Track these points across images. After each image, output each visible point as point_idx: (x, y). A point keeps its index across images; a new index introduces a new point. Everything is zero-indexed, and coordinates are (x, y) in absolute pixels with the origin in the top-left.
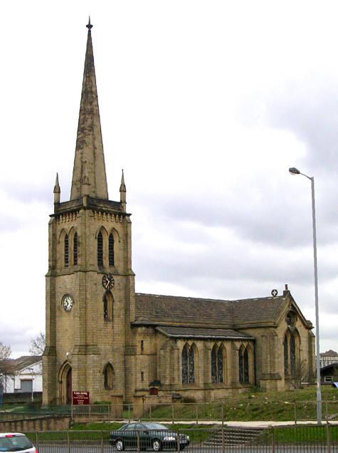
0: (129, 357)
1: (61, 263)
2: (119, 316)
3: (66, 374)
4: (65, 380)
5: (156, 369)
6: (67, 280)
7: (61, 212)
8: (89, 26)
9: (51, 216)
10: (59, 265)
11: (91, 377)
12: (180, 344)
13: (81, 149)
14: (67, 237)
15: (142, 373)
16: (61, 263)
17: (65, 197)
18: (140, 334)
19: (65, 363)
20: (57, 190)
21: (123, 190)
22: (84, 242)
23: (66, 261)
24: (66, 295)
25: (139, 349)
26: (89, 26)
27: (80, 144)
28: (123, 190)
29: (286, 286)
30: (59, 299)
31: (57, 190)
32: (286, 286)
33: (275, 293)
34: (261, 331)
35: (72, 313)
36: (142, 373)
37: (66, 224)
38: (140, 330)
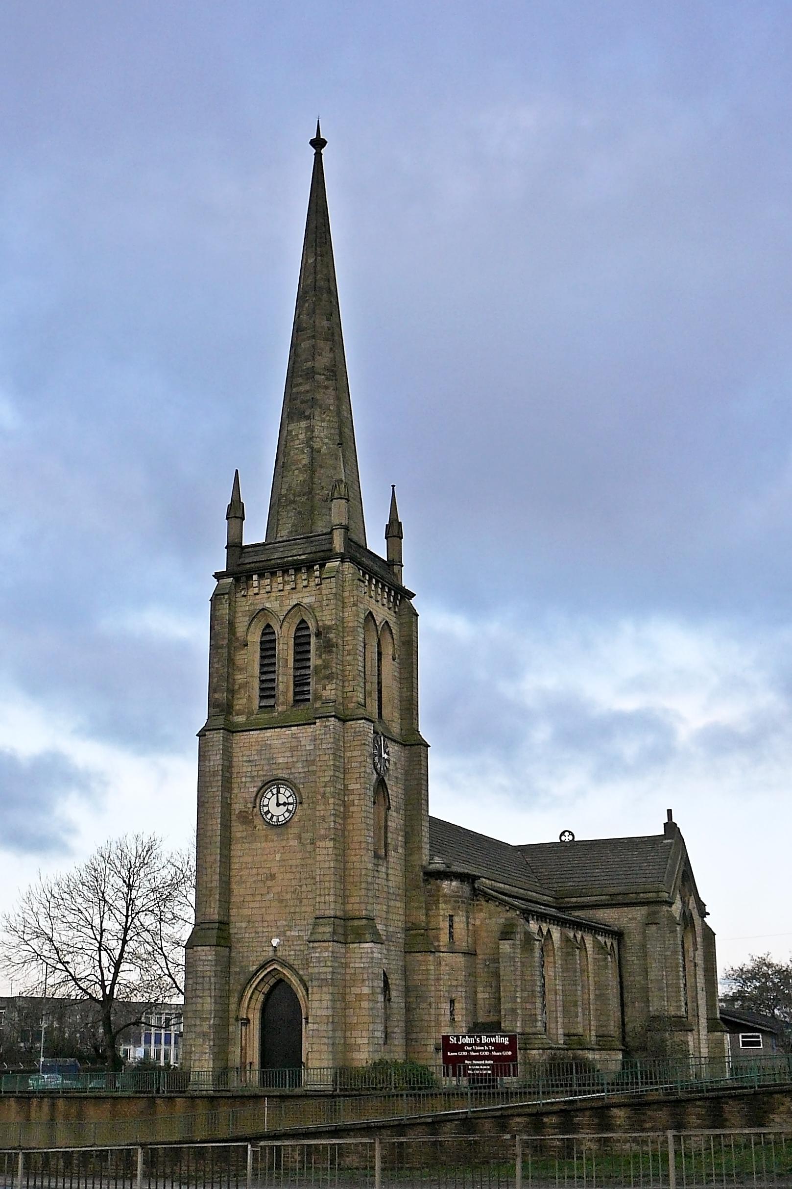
0: (419, 957)
1: (249, 698)
2: (396, 850)
3: (261, 997)
4: (258, 1015)
5: (476, 993)
6: (276, 743)
7: (243, 567)
8: (318, 143)
9: (218, 576)
10: (240, 703)
11: (365, 1004)
12: (164, 1017)
13: (308, 418)
14: (268, 630)
15: (452, 1002)
16: (249, 698)
17: (254, 533)
18: (447, 899)
19: (262, 967)
20: (236, 512)
21: (394, 532)
22: (340, 642)
23: (267, 691)
24: (273, 782)
25: (444, 938)
26: (318, 143)
27: (295, 408)
28: (394, 532)
29: (669, 812)
30: (243, 794)
31: (236, 512)
32: (669, 812)
33: (427, 880)
34: (639, 913)
35: (294, 830)
36: (452, 1002)
37: (273, 596)
38: (449, 887)
